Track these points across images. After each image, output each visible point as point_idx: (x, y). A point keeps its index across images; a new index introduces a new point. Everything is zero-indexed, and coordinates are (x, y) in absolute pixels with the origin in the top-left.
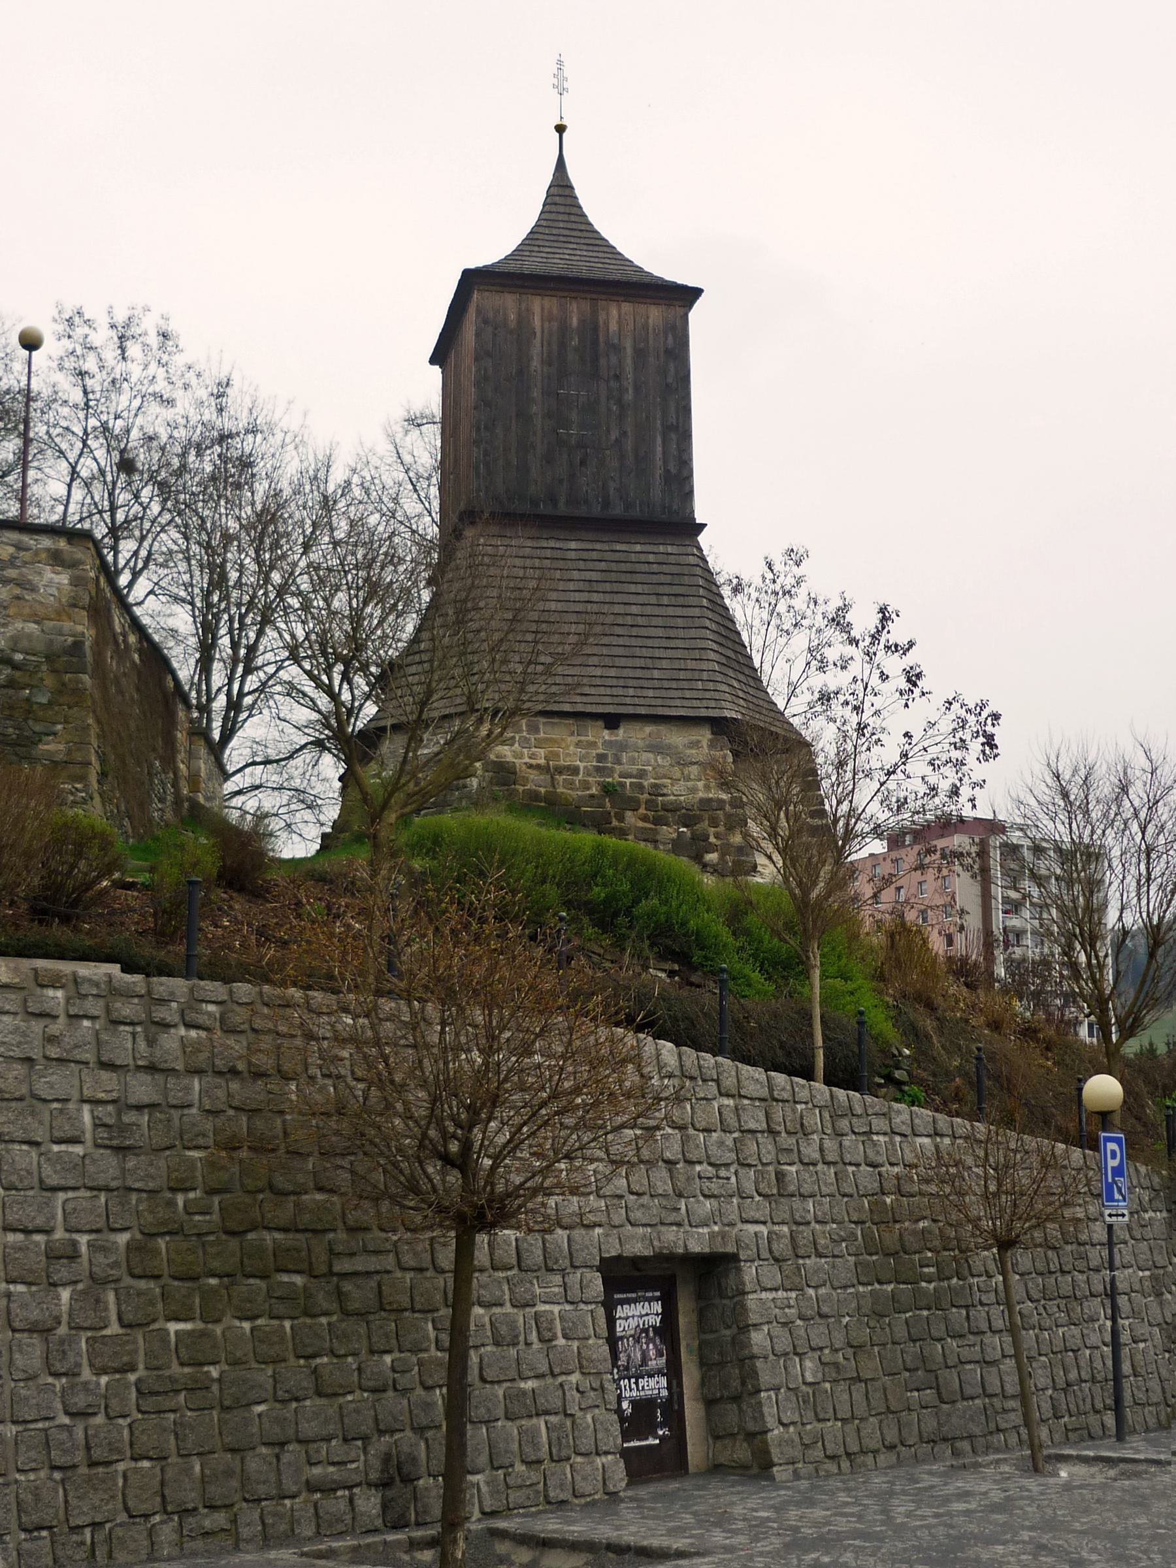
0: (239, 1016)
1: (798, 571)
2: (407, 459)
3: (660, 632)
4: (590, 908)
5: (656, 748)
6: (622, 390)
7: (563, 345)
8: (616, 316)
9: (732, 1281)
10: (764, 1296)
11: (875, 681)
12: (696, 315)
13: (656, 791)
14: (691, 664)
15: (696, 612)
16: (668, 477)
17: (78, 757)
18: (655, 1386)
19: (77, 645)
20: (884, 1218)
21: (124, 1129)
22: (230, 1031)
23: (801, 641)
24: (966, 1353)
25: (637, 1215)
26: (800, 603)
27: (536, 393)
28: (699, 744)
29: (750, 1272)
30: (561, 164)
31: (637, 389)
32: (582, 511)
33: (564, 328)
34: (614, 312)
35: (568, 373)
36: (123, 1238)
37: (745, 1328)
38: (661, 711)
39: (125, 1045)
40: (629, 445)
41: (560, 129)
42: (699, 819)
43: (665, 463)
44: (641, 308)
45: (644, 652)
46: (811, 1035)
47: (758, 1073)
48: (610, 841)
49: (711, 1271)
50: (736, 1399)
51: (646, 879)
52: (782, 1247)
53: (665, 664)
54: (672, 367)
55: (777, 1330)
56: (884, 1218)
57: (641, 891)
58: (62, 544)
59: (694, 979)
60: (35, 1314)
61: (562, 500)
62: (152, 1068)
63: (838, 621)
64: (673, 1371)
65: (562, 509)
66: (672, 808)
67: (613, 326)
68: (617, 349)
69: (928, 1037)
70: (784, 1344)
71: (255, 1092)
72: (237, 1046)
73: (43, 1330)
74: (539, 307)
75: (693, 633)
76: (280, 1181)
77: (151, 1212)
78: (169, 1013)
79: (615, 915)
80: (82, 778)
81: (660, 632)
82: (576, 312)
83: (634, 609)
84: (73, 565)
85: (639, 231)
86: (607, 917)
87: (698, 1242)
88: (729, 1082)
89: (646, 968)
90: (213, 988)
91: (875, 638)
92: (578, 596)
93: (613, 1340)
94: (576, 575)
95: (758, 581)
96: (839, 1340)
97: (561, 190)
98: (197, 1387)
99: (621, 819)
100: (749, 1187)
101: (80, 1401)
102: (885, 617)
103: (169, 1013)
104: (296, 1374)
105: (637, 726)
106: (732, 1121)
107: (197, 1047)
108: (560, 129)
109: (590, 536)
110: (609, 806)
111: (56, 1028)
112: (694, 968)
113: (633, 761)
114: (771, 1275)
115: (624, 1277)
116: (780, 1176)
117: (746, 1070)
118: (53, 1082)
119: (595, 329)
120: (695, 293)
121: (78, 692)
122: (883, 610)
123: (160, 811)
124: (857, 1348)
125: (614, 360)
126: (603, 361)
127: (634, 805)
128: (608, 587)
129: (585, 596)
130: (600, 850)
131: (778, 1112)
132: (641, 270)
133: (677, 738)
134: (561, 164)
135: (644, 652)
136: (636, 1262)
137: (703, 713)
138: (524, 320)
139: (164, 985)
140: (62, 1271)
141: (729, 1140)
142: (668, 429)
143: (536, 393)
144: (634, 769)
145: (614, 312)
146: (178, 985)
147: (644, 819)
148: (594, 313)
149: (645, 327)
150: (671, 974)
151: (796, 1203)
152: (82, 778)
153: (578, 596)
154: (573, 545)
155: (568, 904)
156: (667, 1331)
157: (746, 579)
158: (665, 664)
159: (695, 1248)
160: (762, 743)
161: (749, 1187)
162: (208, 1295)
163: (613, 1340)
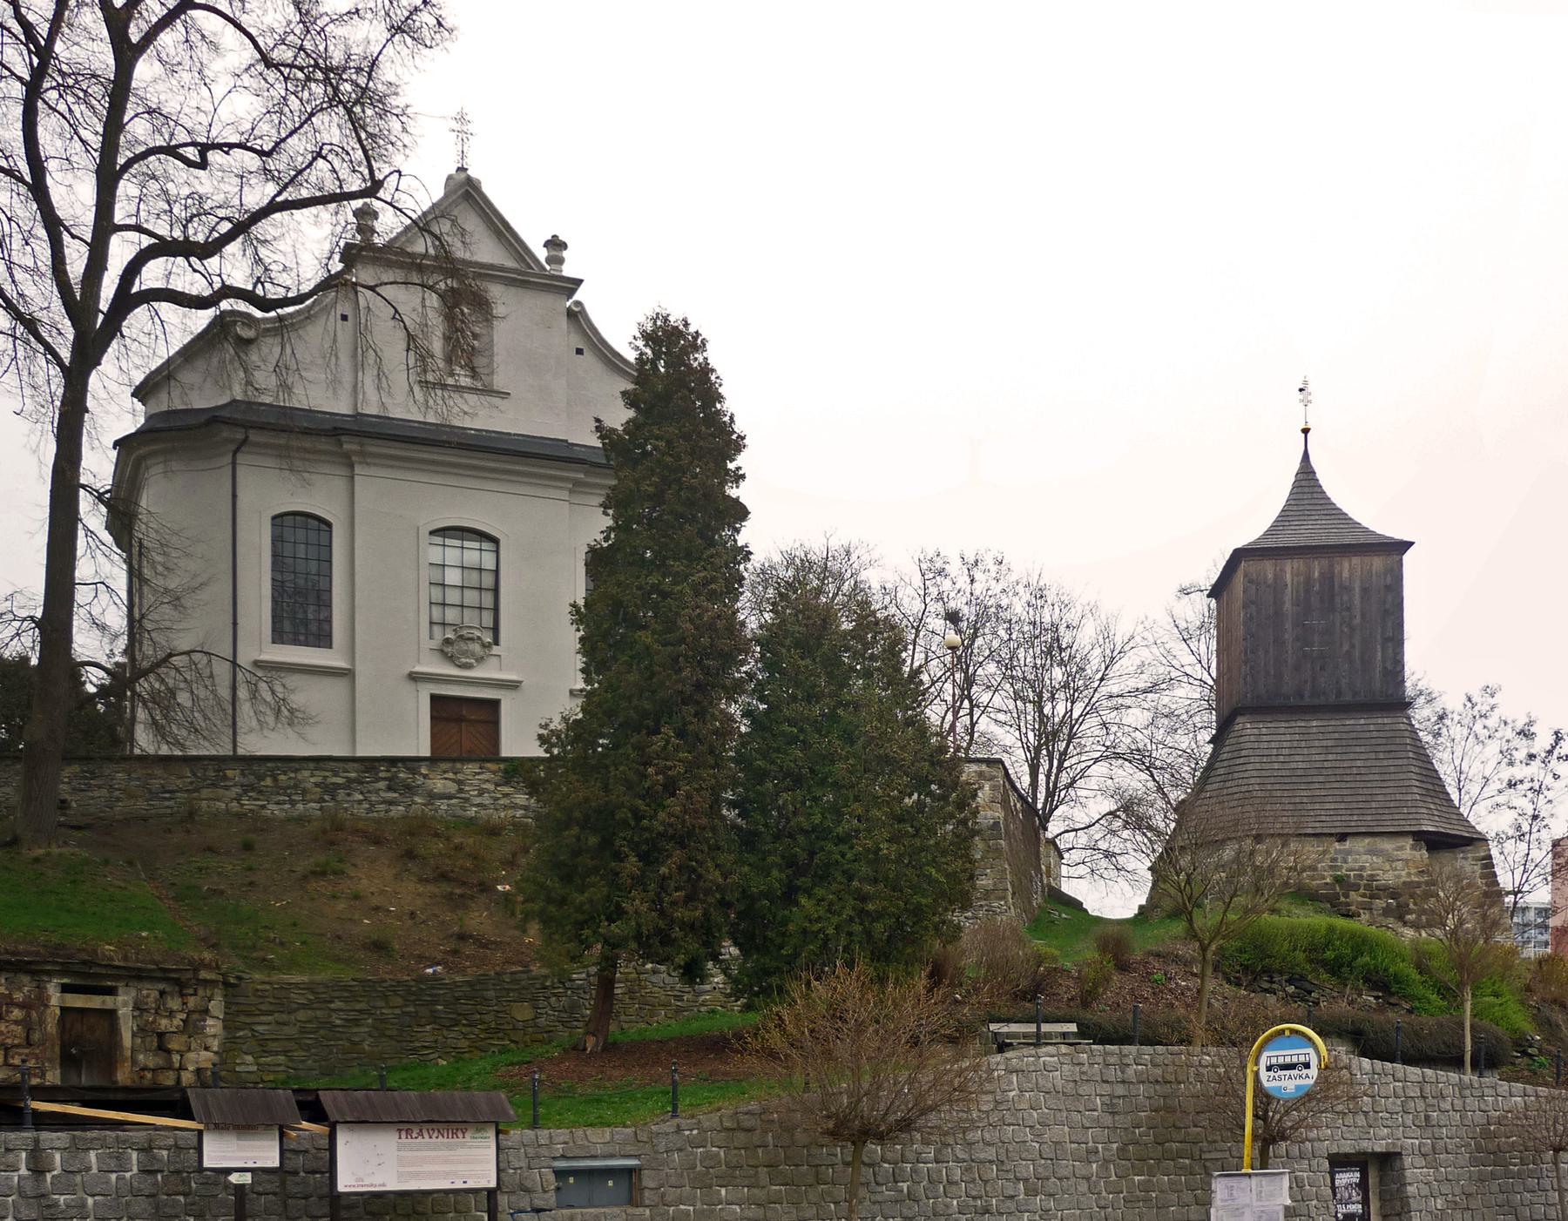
0: (1159, 1060)
1: (1492, 701)
2: (1183, 625)
3: (1377, 777)
4: (1324, 963)
5: (1371, 852)
6: (1352, 617)
7: (1307, 591)
8: (1347, 568)
9: (1398, 1163)
10: (1415, 1172)
11: (1549, 780)
12: (1408, 558)
13: (1372, 878)
14: (1399, 797)
15: (1405, 762)
16: (1386, 673)
17: (1000, 886)
18: (1356, 1208)
19: (996, 824)
20: (1487, 1135)
21: (1113, 1105)
22: (1155, 1065)
23: (1493, 748)
24: (1535, 1200)
25: (1347, 1135)
26: (1492, 722)
27: (1288, 626)
28: (1407, 850)
29: (1408, 1161)
30: (1306, 456)
31: (1363, 616)
32: (1322, 701)
33: (1308, 581)
34: (1346, 565)
35: (1311, 619)
36: (1115, 1146)
37: (1405, 1185)
38: (1376, 830)
39: (1111, 1074)
40: (1357, 653)
41: (1306, 431)
42: (1400, 895)
43: (1384, 661)
44: (1367, 560)
45: (1365, 791)
46: (1463, 1036)
47: (1417, 1070)
48: (1341, 922)
49: (1387, 1161)
50: (1399, 1215)
51: (1361, 944)
52: (1427, 1149)
53: (1380, 798)
54: (1390, 598)
55: (1422, 1186)
56: (1487, 1135)
57: (1358, 951)
58: (984, 767)
59: (1392, 1000)
60: (1084, 1172)
61: (1307, 694)
62: (1123, 1082)
63: (1526, 734)
64: (1365, 1202)
65: (1307, 701)
66: (1385, 889)
67: (1346, 574)
68: (1348, 589)
69: (1558, 1026)
70: (1425, 1191)
71: (1167, 1089)
72: (1159, 1071)
73: (1088, 1179)
74: (1290, 568)
75: (1402, 776)
76: (1178, 1124)
77: (206, 1011)
78: (1130, 1060)
79: (1342, 966)
80: (1004, 898)
81: (1377, 777)
82: (1317, 568)
83: (1359, 763)
84: (992, 778)
85: (1365, 503)
86: (1335, 968)
87: (1379, 1147)
88: (1400, 1075)
89: (1360, 995)
90: (1147, 1049)
91: (1550, 752)
92: (1317, 758)
93: (1333, 1188)
94: (1317, 743)
95: (1460, 708)
96: (1457, 1191)
97: (1306, 474)
98: (1147, 1200)
99: (1347, 896)
100: (1409, 1122)
101: (1103, 1203)
102: (1558, 737)
103: (1130, 1060)
104: (1188, 1197)
105: (1359, 839)
106: (1400, 1092)
107: (1142, 1072)
108: (1306, 431)
109: (1327, 716)
110: (1334, 898)
111: (1084, 1069)
112: (1392, 994)
113: (1356, 861)
114: (1421, 1162)
115: (1339, 1162)
116: (1427, 1118)
117: (1410, 1069)
118: (1085, 1089)
119: (1332, 578)
120: (1406, 546)
121: (998, 850)
122: (1556, 733)
123: (1037, 900)
124: (1468, 1195)
125: (1346, 598)
126: (1338, 600)
127: (1356, 887)
128: (1339, 750)
129: (1322, 757)
130: (1331, 929)
131: (1427, 1088)
132: (1366, 530)
133: (1387, 845)
134: (1306, 456)
135: (1365, 791)
136: (1347, 1155)
137: (1408, 829)
138: (1279, 577)
139: (1126, 1049)
140: (1093, 1158)
141: (1398, 1102)
142: (1386, 640)
143: (1288, 626)
144: (1357, 866)
145: (1346, 565)
146: (1133, 1049)
147: (1364, 896)
148: (1331, 566)
149: (1370, 572)
150: (1377, 998)
151: (1436, 1129)
152: (1004, 898)
153: (1317, 758)
154: (1315, 723)
155: (1311, 961)
156: (1363, 1185)
157: (1449, 708)
158: (1380, 798)
159: (1378, 1149)
160: (1454, 840)
161: (1409, 1122)
162: (1150, 1168)
163: (1333, 1188)
